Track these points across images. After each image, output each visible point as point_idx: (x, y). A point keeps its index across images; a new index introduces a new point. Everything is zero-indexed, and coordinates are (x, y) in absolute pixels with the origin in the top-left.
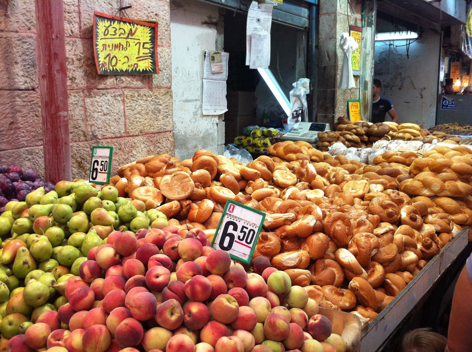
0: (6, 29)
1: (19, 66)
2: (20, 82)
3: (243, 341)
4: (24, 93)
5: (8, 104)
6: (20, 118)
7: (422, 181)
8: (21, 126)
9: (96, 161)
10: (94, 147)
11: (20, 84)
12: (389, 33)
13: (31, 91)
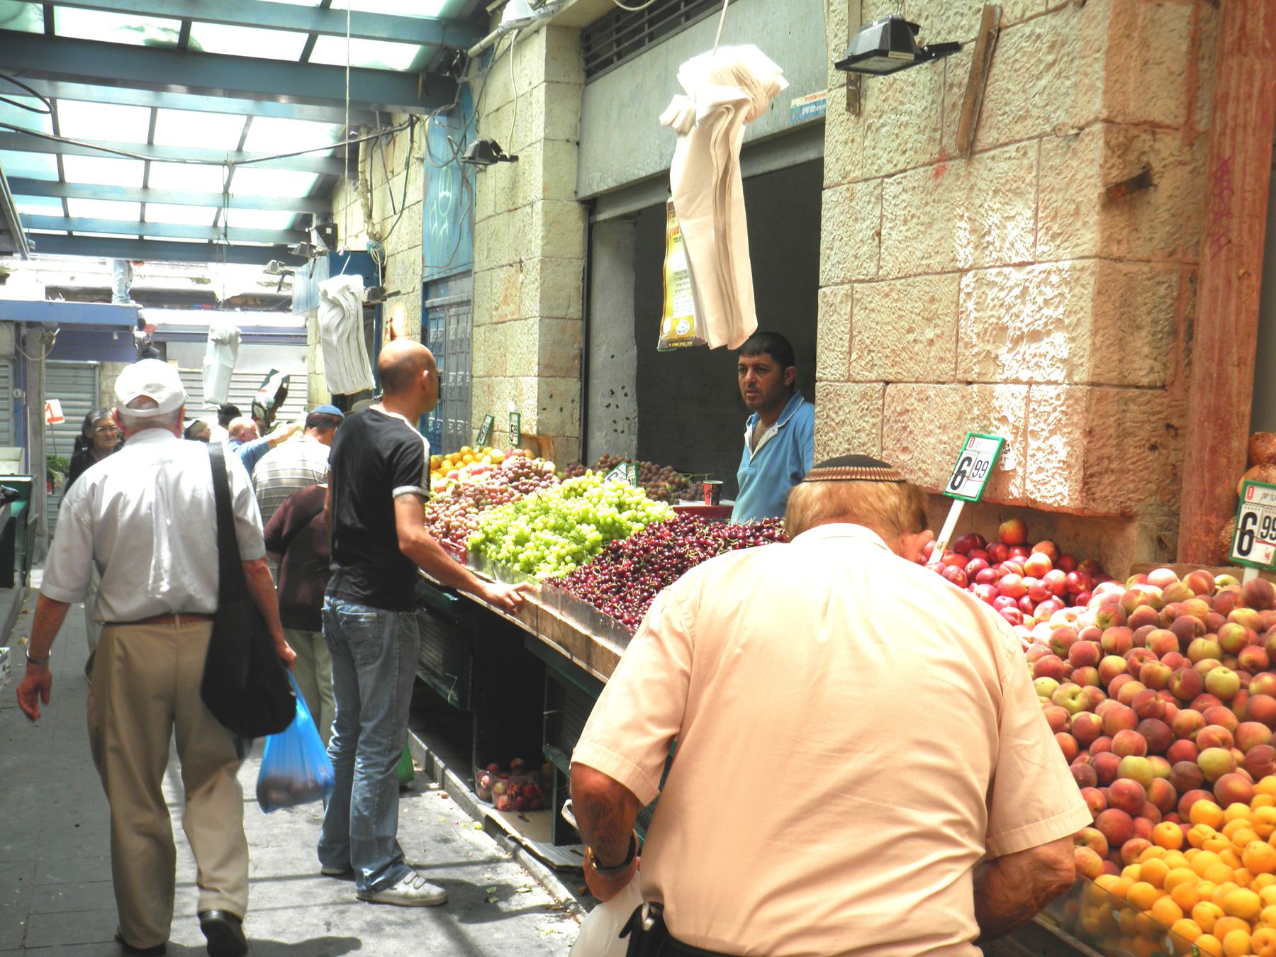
0: (1129, 256)
1: (1144, 333)
2: (1141, 369)
3: (568, 141)
4: (1145, 394)
5: (1113, 416)
6: (1131, 450)
7: (1095, 257)
8: (1131, 467)
9: (969, 459)
10: (973, 436)
11: (1142, 373)
12: (633, 335)
13: (1159, 392)
